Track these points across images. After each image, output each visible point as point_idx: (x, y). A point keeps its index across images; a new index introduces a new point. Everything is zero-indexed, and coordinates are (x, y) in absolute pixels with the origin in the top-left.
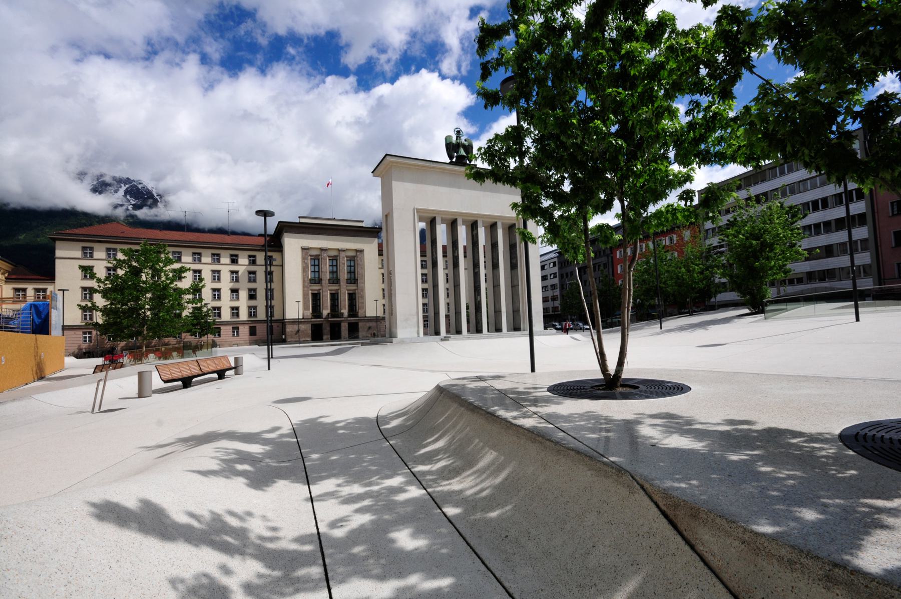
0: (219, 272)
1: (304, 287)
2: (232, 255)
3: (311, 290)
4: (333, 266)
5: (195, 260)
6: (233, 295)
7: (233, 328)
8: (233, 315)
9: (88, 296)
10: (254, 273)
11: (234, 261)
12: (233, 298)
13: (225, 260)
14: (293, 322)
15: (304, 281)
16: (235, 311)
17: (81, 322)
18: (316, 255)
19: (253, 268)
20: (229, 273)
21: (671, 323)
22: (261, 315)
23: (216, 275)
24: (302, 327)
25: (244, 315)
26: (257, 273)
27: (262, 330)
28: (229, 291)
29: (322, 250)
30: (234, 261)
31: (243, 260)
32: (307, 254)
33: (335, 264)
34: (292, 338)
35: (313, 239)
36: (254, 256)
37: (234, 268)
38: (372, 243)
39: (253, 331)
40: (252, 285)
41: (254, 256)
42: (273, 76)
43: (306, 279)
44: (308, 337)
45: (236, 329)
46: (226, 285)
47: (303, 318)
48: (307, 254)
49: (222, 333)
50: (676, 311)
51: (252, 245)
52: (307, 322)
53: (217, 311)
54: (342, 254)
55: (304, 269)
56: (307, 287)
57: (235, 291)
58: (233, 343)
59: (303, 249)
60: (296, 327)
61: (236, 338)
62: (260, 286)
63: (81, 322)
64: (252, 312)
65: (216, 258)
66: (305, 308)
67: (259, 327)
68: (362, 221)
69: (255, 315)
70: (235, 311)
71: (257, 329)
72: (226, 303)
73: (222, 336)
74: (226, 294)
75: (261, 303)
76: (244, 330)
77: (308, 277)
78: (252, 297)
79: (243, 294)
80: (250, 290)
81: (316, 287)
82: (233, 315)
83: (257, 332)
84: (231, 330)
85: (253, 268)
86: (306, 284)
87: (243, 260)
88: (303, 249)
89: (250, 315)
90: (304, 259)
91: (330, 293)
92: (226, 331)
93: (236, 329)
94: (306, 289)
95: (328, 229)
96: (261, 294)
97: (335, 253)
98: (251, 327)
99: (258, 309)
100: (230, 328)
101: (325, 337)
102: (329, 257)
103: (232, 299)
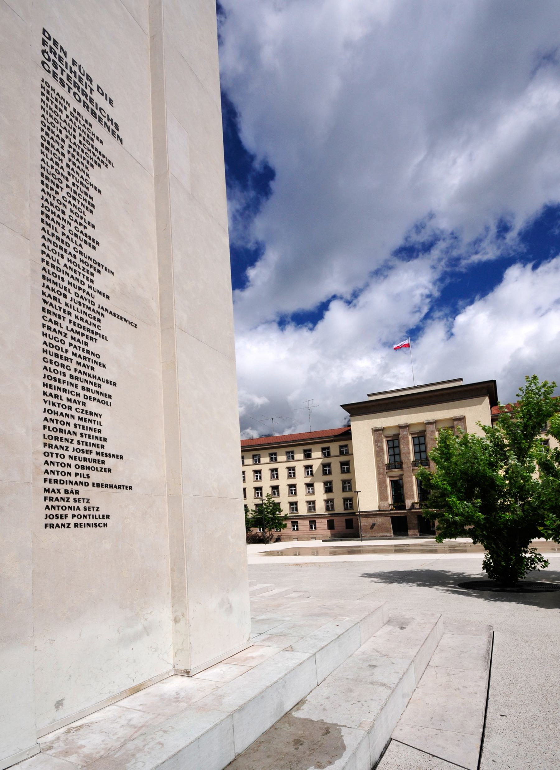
0: (293, 468)
1: (379, 473)
2: (305, 451)
3: (390, 477)
4: (419, 444)
5: (272, 460)
6: (309, 489)
7: (310, 521)
8: (310, 509)
9: (550, 484)
10: (329, 465)
11: (308, 456)
12: (309, 492)
13: (299, 456)
14: (366, 515)
15: (378, 468)
16: (311, 504)
17: (325, 512)
18: (394, 435)
19: (328, 460)
20: (303, 468)
21: (505, 276)
22: (339, 507)
23: (292, 472)
24: (379, 520)
25: (320, 507)
26: (332, 465)
27: (340, 523)
28: (305, 486)
29: (401, 427)
30: (308, 456)
31: (317, 454)
32: (379, 436)
33: (422, 440)
34: (366, 532)
35: (387, 417)
36: (328, 448)
37: (308, 462)
38: (481, 403)
39: (331, 525)
40: (327, 478)
41: (328, 448)
42: (260, 259)
43: (381, 465)
44: (388, 531)
45: (313, 523)
46: (301, 480)
47: (379, 510)
48: (379, 436)
49: (299, 527)
50: (402, 489)
51: (322, 438)
52: (386, 515)
53: (294, 506)
54: (430, 428)
55: (379, 453)
56: (383, 474)
57: (310, 485)
58: (294, 537)
59: (375, 431)
60: (371, 521)
61: (313, 532)
62: (337, 477)
63: (325, 512)
64: (329, 504)
65: (290, 456)
66: (382, 496)
67: (336, 520)
68: (461, 380)
69: (333, 509)
70: (311, 504)
71: (335, 523)
72: (302, 497)
73: (299, 529)
74: (301, 489)
75: (338, 496)
76: (322, 524)
77: (383, 462)
78: (328, 489)
79: (319, 487)
80: (326, 483)
81: (396, 473)
82: (310, 510)
83: (335, 526)
84: (309, 524)
85: (328, 460)
86: (381, 470)
87: (317, 454)
88: (375, 431)
89: (327, 508)
90: (377, 442)
91: (391, 481)
92: (304, 525)
93: (313, 523)
94: (381, 476)
95: (363, 407)
96: (337, 486)
97: (421, 428)
98: (347, 520)
99: (335, 501)
100: (307, 522)
101: (410, 532)
102: (412, 434)
103: (308, 493)
